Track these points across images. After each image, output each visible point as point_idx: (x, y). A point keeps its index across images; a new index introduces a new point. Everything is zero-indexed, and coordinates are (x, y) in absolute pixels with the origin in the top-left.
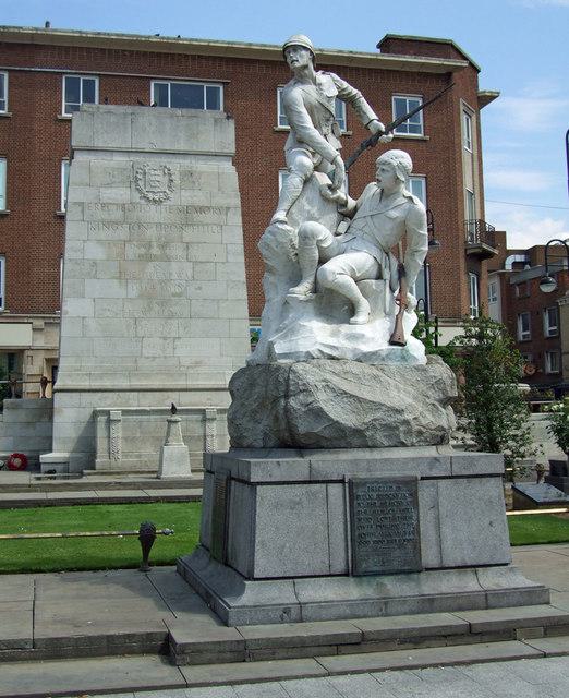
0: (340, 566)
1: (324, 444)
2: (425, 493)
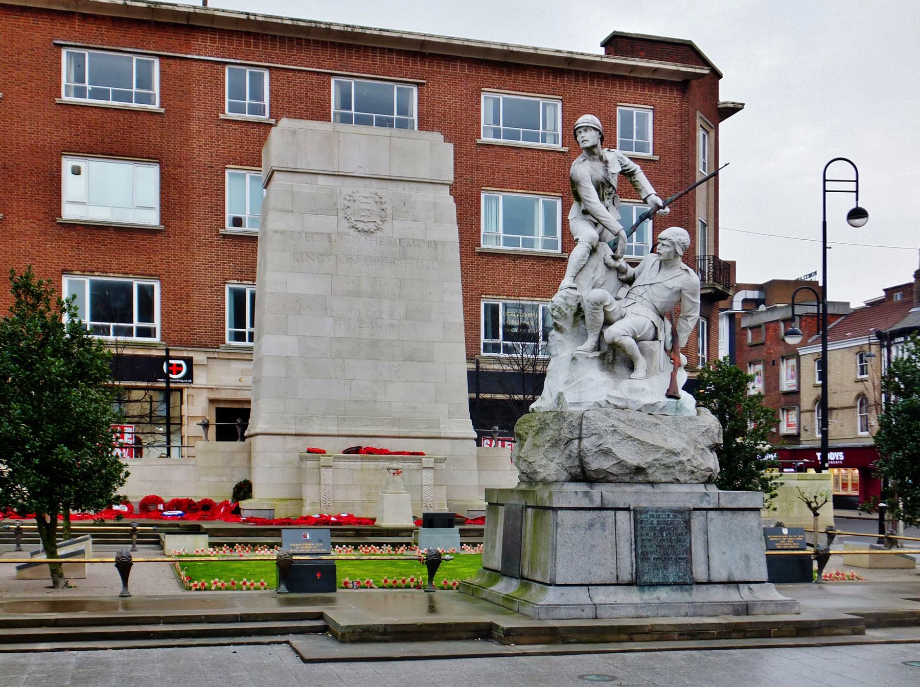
0: (626, 576)
1: (611, 478)
2: (697, 521)
